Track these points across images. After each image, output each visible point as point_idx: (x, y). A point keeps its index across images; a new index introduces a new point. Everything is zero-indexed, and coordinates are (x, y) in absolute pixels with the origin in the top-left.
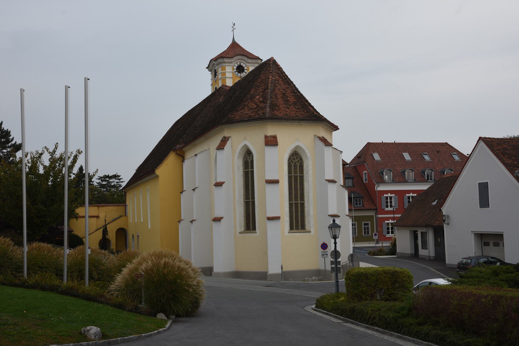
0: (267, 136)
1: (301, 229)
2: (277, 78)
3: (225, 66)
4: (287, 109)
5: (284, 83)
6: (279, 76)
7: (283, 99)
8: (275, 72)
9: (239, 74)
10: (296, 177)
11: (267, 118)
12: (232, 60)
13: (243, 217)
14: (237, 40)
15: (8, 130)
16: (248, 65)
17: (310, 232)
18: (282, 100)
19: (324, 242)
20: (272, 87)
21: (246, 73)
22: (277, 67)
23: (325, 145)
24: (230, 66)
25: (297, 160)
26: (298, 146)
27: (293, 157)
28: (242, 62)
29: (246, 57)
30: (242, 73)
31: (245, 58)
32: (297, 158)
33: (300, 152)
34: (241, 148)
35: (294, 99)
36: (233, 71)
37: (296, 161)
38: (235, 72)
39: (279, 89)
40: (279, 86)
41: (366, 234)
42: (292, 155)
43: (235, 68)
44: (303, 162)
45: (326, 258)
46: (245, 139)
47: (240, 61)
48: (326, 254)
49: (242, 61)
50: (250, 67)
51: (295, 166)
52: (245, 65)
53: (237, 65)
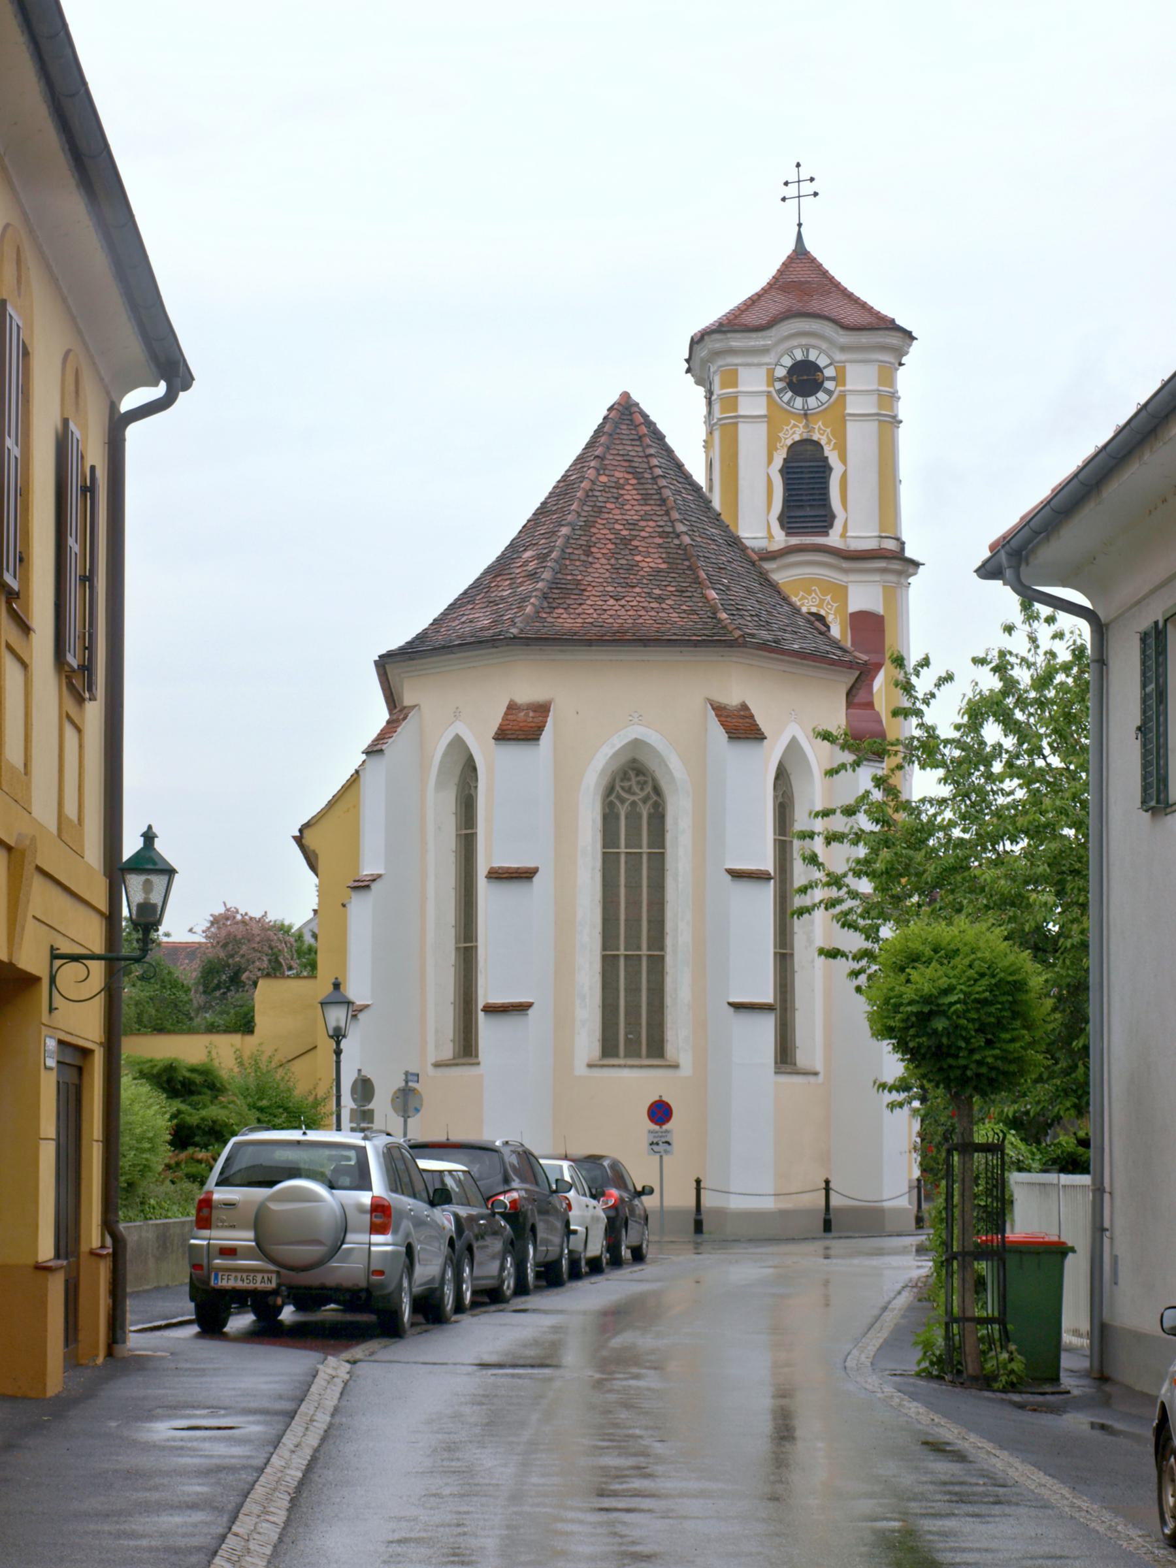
0: (516, 704)
2: (621, 475)
3: (737, 365)
4: (612, 602)
6: (630, 470)
7: (613, 561)
8: (618, 454)
9: (799, 402)
11: (511, 638)
12: (764, 338)
13: (452, 1007)
14: (809, 246)
16: (839, 356)
17: (676, 1066)
18: (608, 567)
19: (661, 1096)
20: (586, 514)
21: (829, 393)
22: (633, 432)
23: (729, 737)
24: (759, 365)
25: (642, 795)
26: (636, 739)
27: (626, 784)
28: (814, 347)
29: (831, 324)
31: (827, 329)
32: (642, 784)
33: (652, 765)
34: (446, 750)
35: (660, 561)
36: (771, 389)
37: (635, 798)
38: (779, 392)
40: (617, 511)
41: (616, 1055)
42: (625, 773)
43: (781, 372)
44: (663, 801)
45: (665, 1158)
46: (457, 714)
48: (664, 1140)
49: (813, 341)
50: (849, 367)
52: (829, 357)
53: (787, 362)
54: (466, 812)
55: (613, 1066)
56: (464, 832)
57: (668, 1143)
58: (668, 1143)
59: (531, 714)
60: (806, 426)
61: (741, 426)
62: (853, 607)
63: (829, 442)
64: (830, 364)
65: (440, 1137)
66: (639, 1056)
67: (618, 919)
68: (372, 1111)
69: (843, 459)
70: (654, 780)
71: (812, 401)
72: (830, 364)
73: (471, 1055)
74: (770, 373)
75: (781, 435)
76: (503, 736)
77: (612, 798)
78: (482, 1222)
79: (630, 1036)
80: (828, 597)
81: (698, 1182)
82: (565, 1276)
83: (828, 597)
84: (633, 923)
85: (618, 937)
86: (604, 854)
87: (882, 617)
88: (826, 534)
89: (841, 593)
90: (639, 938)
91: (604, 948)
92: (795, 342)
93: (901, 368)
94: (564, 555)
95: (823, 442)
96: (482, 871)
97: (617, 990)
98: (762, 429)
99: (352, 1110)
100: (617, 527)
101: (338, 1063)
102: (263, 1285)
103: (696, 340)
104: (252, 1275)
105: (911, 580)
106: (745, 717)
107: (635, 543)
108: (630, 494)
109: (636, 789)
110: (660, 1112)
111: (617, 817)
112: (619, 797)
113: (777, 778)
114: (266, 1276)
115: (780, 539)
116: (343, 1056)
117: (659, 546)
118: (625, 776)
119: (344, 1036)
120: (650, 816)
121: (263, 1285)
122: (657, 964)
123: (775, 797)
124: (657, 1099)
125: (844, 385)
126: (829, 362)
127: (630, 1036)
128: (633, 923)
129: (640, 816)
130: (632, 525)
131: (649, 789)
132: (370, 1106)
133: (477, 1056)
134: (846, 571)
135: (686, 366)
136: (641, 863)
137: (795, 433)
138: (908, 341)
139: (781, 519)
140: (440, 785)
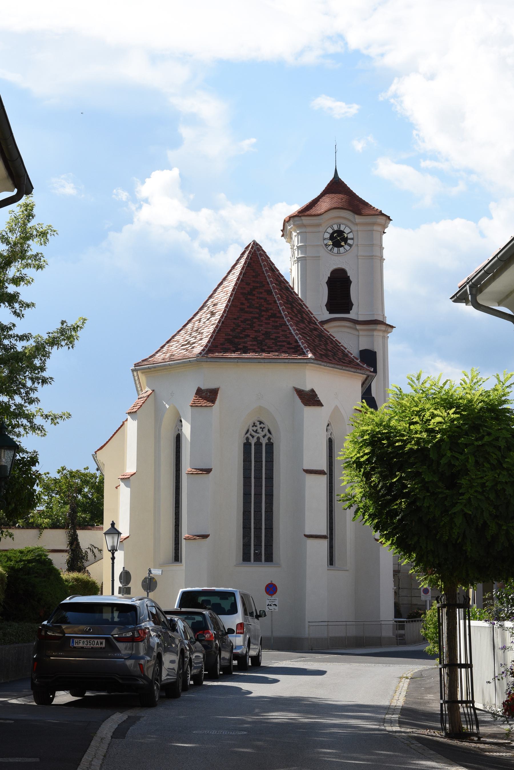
0: (201, 389)
14: (341, 176)
16: (354, 228)
25: (263, 434)
27: (255, 428)
48: (274, 603)
59: (209, 394)
64: (351, 232)
65: (499, 251)
72: (351, 232)
73: (178, 561)
77: (248, 435)
79: (257, 552)
82: (180, 691)
88: (349, 313)
93: (384, 234)
99: (120, 588)
101: (113, 563)
102: (97, 646)
103: (287, 220)
104: (92, 640)
105: (389, 335)
109: (260, 430)
114: (99, 641)
115: (326, 315)
116: (115, 561)
119: (116, 550)
121: (97, 646)
124: (270, 582)
127: (257, 552)
131: (266, 431)
132: (129, 586)
135: (282, 233)
138: (388, 221)
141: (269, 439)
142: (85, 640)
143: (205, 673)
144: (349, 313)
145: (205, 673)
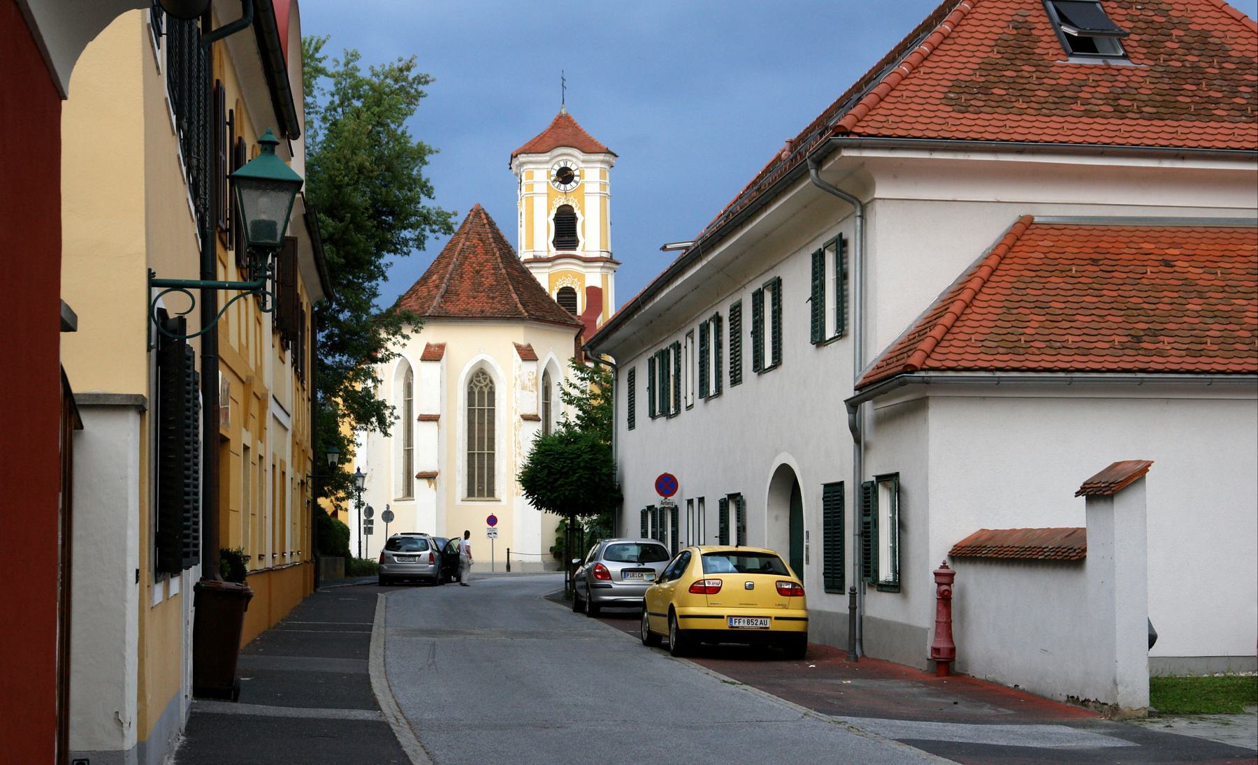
1: (488, 496)
5: (1145, 51)
10: (481, 411)
15: (428, 180)
17: (500, 501)
21: (577, 183)
27: (478, 379)
30: (561, 182)
33: (489, 371)
36: (549, 180)
39: (471, 264)
41: (474, 496)
43: (554, 172)
47: (565, 158)
51: (481, 393)
52: (576, 165)
53: (557, 168)
54: (408, 391)
55: (472, 501)
56: (407, 399)
57: (495, 533)
58: (495, 533)
60: (566, 198)
61: (535, 198)
62: (588, 284)
63: (576, 206)
66: (484, 496)
67: (474, 437)
68: (372, 520)
69: (583, 214)
70: (490, 377)
71: (568, 186)
74: (549, 173)
75: (554, 202)
76: (424, 359)
77: (472, 385)
78: (261, 650)
80: (576, 280)
81: (508, 550)
83: (576, 280)
84: (481, 439)
85: (474, 444)
86: (469, 409)
87: (601, 289)
88: (575, 249)
89: (581, 277)
90: (484, 445)
91: (469, 450)
92: (560, 158)
94: (449, 279)
95: (574, 206)
96: (415, 416)
97: (474, 468)
98: (545, 199)
100: (474, 265)
103: (514, 155)
106: (529, 350)
107: (482, 273)
108: (479, 250)
109: (482, 381)
110: (492, 520)
111: (474, 393)
112: (475, 384)
113: (544, 376)
115: (554, 252)
117: (493, 274)
118: (477, 376)
120: (488, 393)
122: (492, 457)
123: (543, 384)
125: (583, 179)
126: (576, 168)
128: (481, 439)
129: (484, 393)
130: (480, 264)
131: (488, 381)
133: (413, 496)
134: (585, 267)
136: (484, 413)
137: (561, 201)
139: (553, 242)
140: (396, 378)
141: (491, 388)
142: (746, 619)
143: (486, 448)
144: (576, 250)
145: (486, 448)
